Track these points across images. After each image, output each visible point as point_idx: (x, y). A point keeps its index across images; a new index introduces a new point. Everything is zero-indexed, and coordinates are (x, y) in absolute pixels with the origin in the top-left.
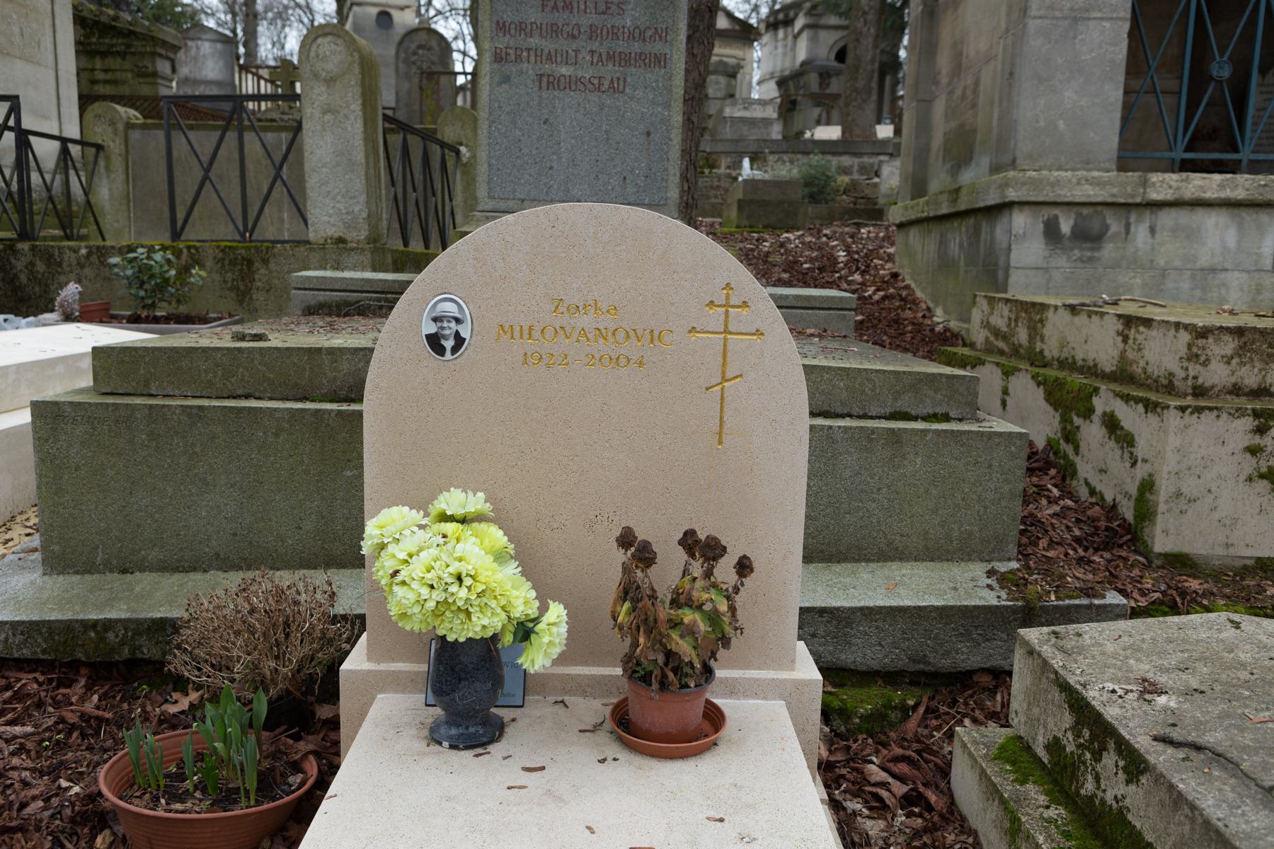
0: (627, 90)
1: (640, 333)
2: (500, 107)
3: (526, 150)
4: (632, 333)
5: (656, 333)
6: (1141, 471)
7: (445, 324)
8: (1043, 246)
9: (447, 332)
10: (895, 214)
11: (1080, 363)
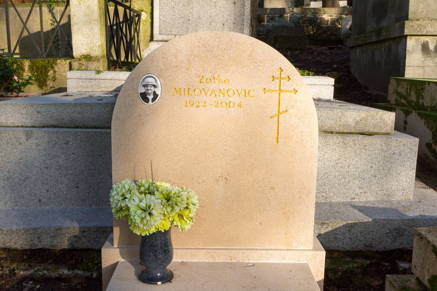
1: (239, 91)
3: (177, 12)
4: (236, 92)
5: (247, 91)
7: (149, 88)
8: (421, 56)
9: (150, 92)
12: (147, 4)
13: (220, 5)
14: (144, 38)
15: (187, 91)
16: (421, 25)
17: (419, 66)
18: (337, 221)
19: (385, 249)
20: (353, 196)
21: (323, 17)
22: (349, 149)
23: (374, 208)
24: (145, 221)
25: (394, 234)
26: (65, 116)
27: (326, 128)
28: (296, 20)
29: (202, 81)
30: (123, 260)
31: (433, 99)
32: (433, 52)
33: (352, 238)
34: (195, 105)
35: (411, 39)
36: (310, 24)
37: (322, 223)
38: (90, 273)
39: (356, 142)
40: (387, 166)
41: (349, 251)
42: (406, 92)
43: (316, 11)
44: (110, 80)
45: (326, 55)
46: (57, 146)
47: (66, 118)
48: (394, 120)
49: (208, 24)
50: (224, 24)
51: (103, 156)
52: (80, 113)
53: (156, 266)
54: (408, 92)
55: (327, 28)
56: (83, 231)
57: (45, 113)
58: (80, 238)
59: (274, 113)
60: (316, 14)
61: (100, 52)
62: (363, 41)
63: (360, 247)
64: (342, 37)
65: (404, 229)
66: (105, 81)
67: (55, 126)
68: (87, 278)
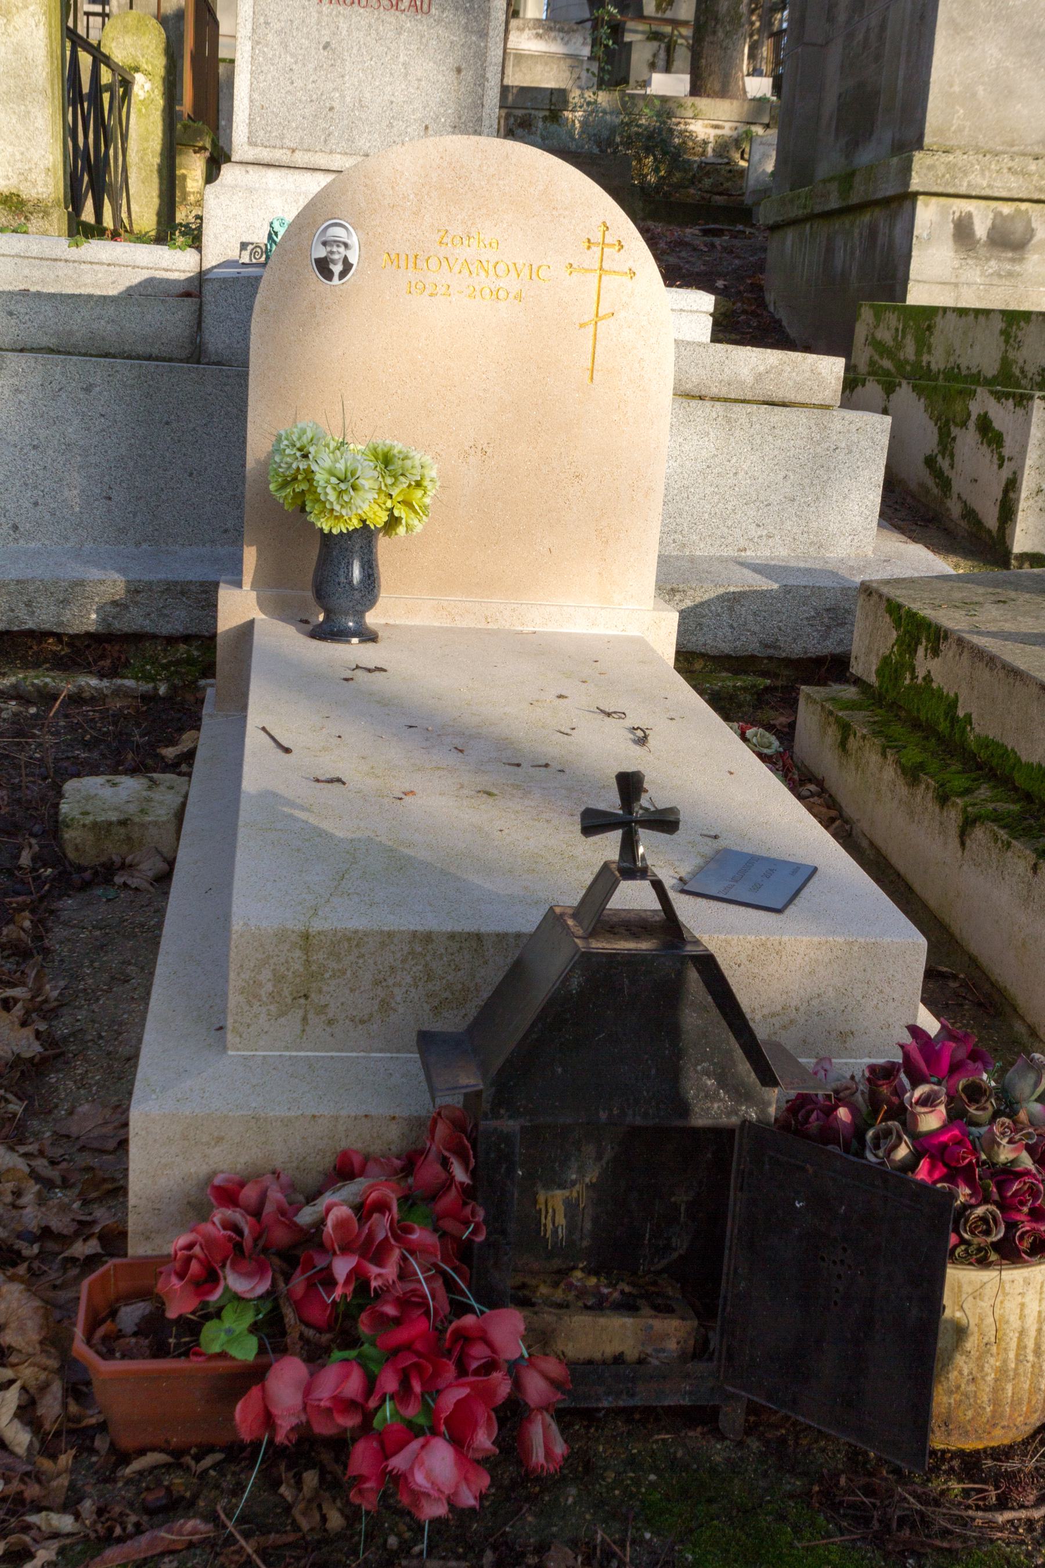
0: (433, 11)
2: (267, 23)
3: (299, 83)
4: (512, 267)
6: (1006, 473)
7: (335, 249)
8: (952, 254)
9: (336, 257)
10: (765, 215)
11: (964, 372)
12: (153, 47)
13: (419, 74)
14: (142, 159)
15: (412, 259)
16: (955, 165)
17: (944, 283)
18: (705, 586)
19: (806, 652)
20: (742, 543)
21: (691, 128)
22: (737, 433)
23: (785, 569)
24: (346, 498)
25: (826, 620)
26: (75, 328)
27: (689, 386)
28: (605, 134)
29: (445, 240)
30: (263, 617)
31: (950, 352)
32: (984, 246)
33: (735, 625)
34: (427, 292)
35: (926, 205)
36: (649, 150)
37: (672, 589)
38: (151, 685)
39: (754, 419)
40: (817, 473)
41: (728, 657)
42: (895, 339)
43: (666, 106)
44: (109, 265)
45: (695, 249)
46: (64, 396)
47: (78, 331)
48: (842, 374)
49: (384, 124)
50: (426, 128)
51: (174, 425)
52: (113, 321)
53: (351, 604)
54: (899, 338)
55: (702, 166)
56: (134, 590)
57: (27, 317)
58: (126, 607)
59: (586, 318)
60: (670, 118)
61: (51, 189)
62: (805, 207)
63: (752, 646)
64: (748, 200)
65: (846, 611)
66: (94, 267)
67: (51, 351)
68: (145, 698)
